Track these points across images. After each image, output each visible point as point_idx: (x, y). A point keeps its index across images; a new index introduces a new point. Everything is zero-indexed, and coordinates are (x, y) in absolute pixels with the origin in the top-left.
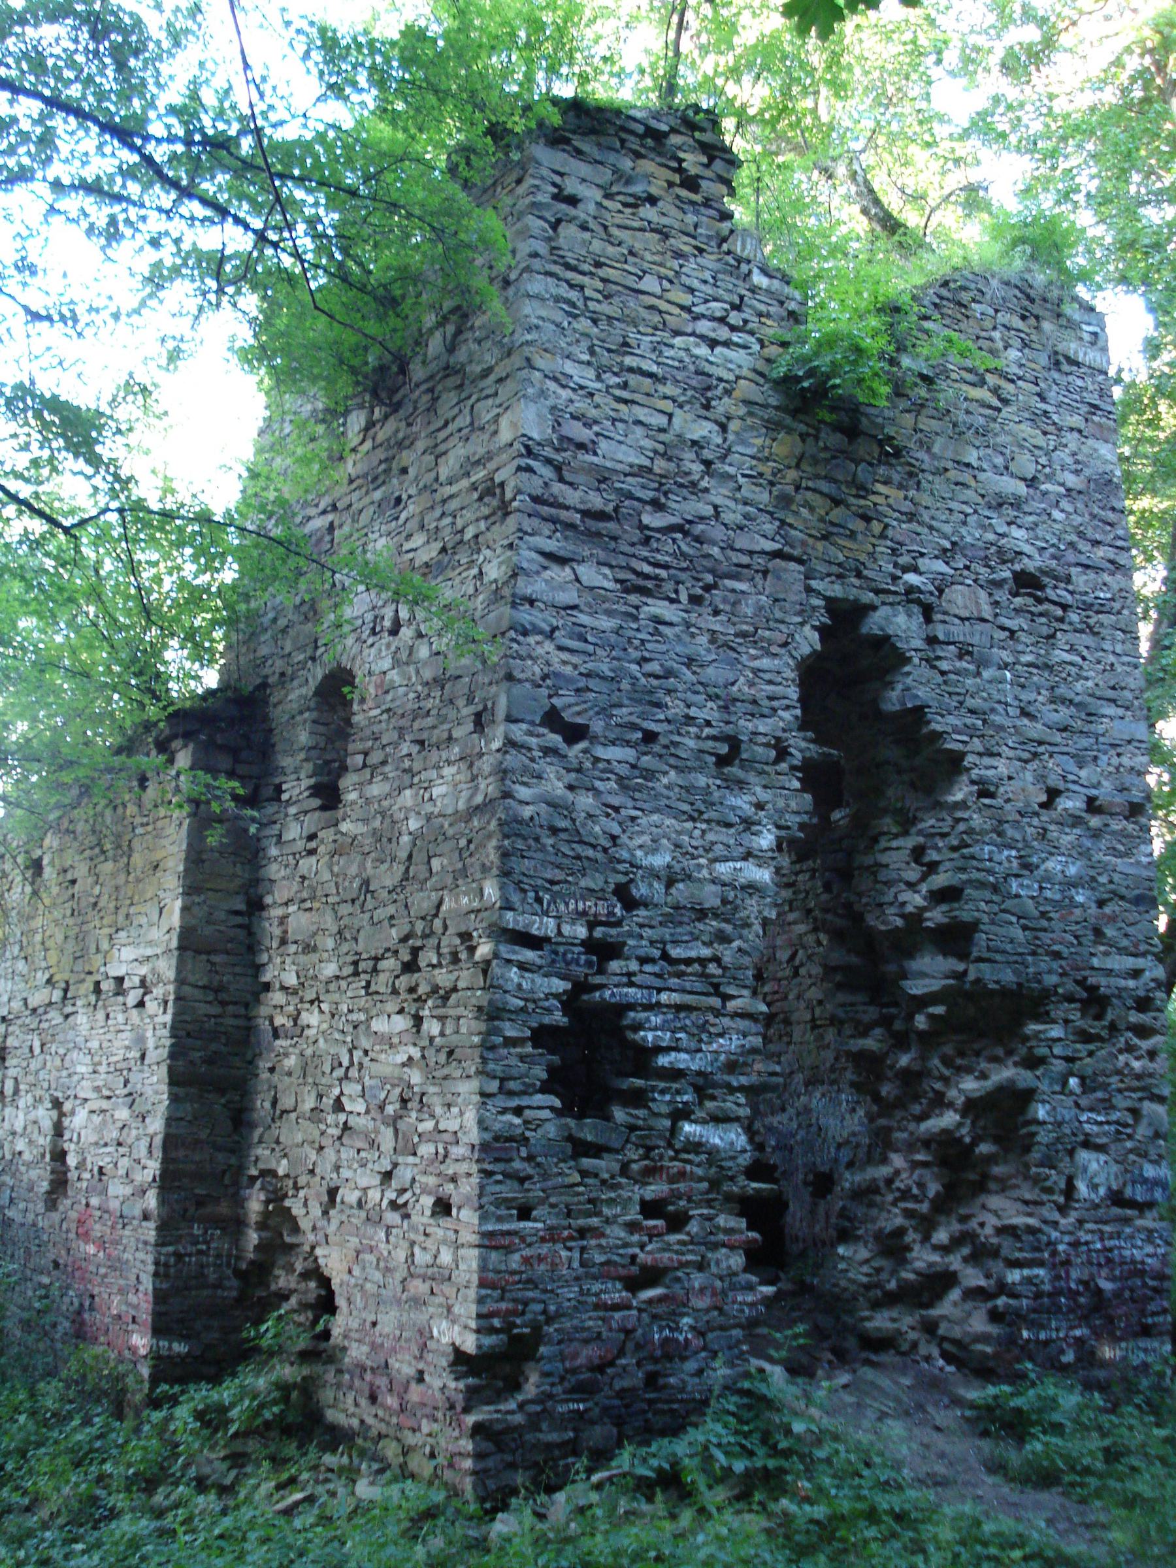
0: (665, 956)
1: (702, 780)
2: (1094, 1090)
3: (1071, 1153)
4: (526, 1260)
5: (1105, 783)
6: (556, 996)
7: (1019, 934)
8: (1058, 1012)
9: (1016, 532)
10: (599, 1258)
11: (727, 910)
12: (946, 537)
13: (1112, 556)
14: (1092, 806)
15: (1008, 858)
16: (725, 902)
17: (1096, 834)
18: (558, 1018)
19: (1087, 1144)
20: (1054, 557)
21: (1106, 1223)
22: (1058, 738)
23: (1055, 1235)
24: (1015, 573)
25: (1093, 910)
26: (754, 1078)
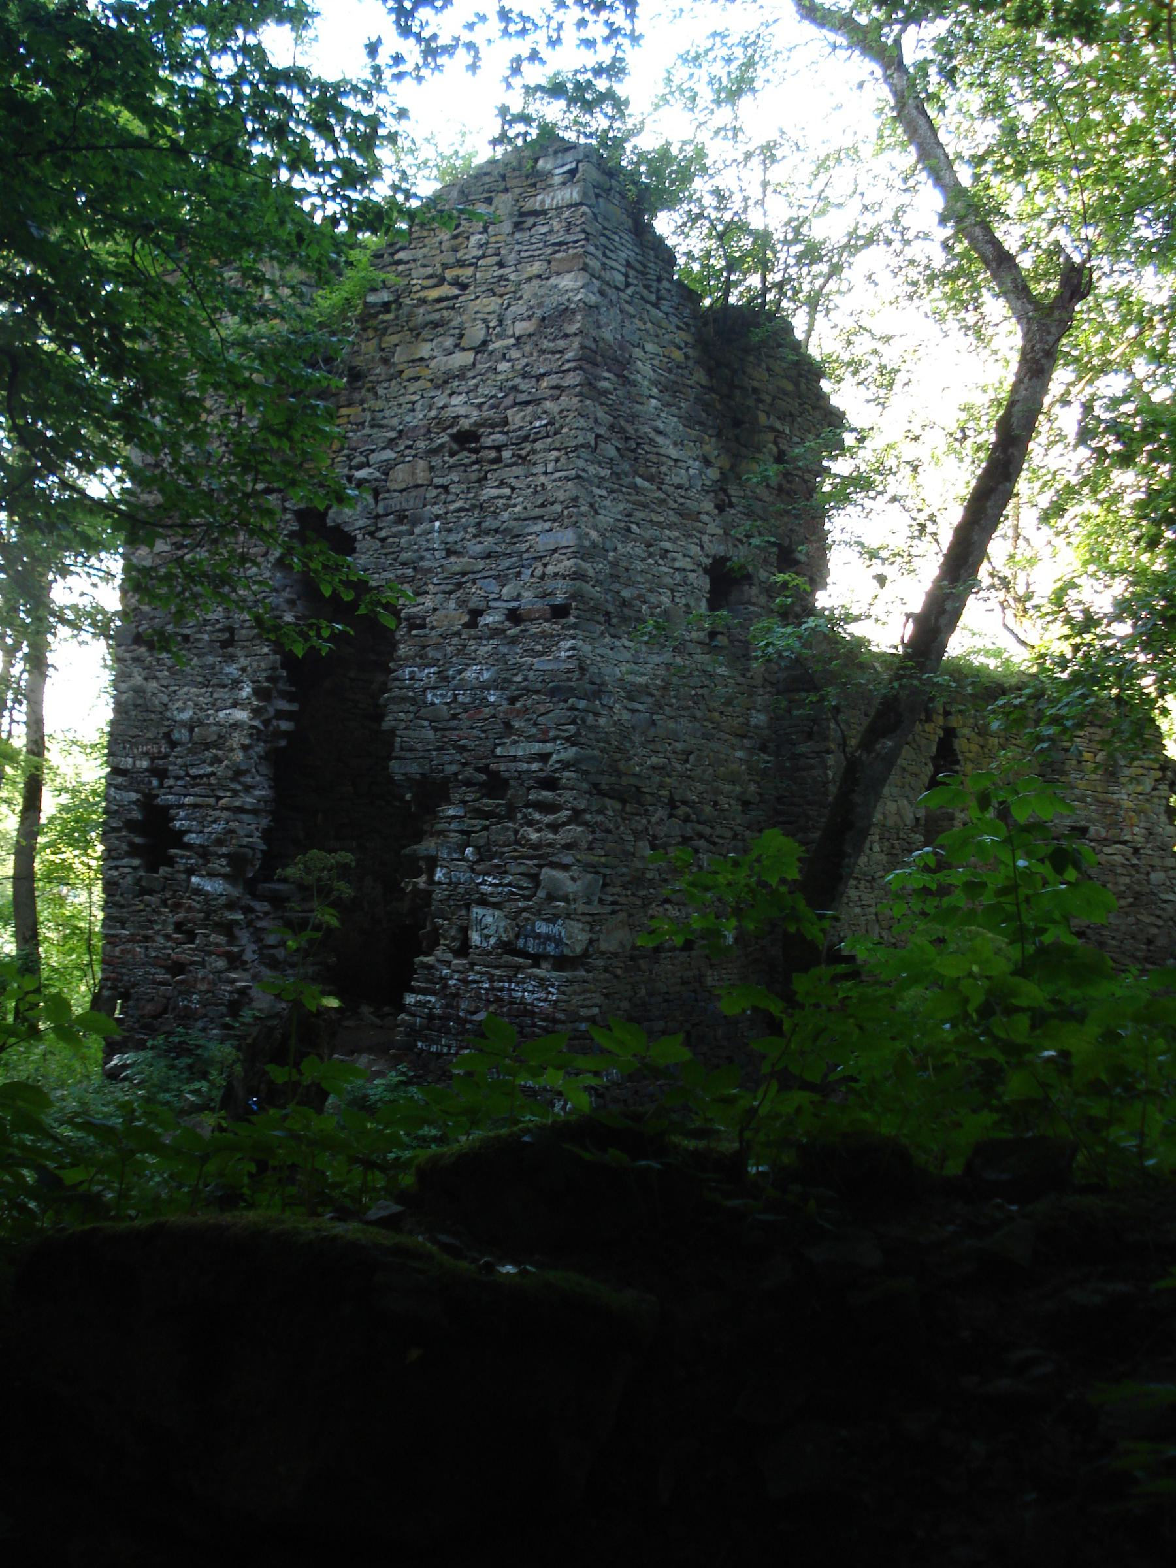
0: (188, 775)
1: (210, 660)
2: (491, 858)
3: (468, 907)
4: (122, 951)
5: (526, 594)
6: (133, 803)
7: (431, 734)
8: (455, 796)
9: (456, 400)
10: (153, 954)
11: (219, 742)
12: (393, 429)
13: (554, 383)
14: (514, 616)
15: (428, 676)
16: (220, 737)
17: (513, 641)
18: (137, 815)
19: (483, 902)
20: (492, 407)
21: (497, 967)
22: (481, 564)
23: (446, 971)
24: (452, 436)
25: (505, 705)
26: (231, 849)
